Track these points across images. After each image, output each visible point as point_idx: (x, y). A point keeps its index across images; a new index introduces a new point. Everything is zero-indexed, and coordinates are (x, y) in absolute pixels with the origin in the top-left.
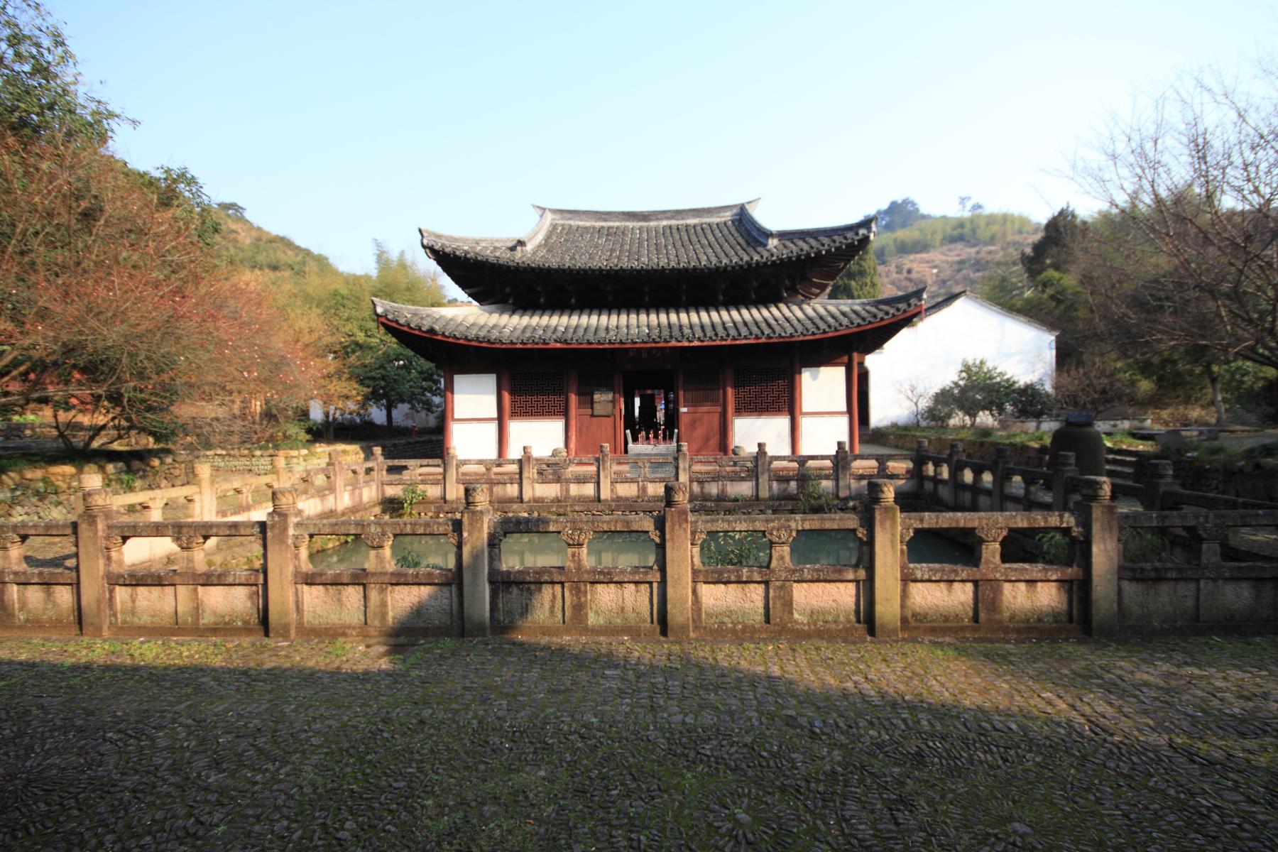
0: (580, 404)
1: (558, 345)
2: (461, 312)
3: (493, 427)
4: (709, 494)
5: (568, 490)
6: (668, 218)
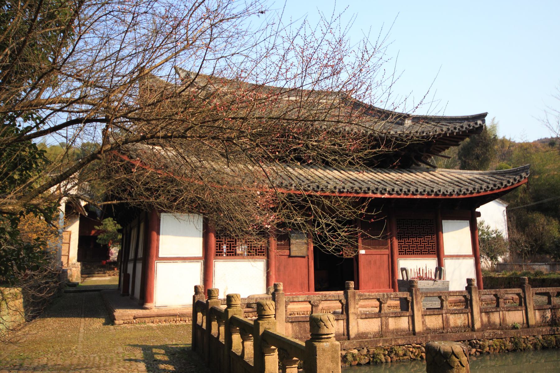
0: (279, 247)
3: (198, 267)
5: (387, 325)
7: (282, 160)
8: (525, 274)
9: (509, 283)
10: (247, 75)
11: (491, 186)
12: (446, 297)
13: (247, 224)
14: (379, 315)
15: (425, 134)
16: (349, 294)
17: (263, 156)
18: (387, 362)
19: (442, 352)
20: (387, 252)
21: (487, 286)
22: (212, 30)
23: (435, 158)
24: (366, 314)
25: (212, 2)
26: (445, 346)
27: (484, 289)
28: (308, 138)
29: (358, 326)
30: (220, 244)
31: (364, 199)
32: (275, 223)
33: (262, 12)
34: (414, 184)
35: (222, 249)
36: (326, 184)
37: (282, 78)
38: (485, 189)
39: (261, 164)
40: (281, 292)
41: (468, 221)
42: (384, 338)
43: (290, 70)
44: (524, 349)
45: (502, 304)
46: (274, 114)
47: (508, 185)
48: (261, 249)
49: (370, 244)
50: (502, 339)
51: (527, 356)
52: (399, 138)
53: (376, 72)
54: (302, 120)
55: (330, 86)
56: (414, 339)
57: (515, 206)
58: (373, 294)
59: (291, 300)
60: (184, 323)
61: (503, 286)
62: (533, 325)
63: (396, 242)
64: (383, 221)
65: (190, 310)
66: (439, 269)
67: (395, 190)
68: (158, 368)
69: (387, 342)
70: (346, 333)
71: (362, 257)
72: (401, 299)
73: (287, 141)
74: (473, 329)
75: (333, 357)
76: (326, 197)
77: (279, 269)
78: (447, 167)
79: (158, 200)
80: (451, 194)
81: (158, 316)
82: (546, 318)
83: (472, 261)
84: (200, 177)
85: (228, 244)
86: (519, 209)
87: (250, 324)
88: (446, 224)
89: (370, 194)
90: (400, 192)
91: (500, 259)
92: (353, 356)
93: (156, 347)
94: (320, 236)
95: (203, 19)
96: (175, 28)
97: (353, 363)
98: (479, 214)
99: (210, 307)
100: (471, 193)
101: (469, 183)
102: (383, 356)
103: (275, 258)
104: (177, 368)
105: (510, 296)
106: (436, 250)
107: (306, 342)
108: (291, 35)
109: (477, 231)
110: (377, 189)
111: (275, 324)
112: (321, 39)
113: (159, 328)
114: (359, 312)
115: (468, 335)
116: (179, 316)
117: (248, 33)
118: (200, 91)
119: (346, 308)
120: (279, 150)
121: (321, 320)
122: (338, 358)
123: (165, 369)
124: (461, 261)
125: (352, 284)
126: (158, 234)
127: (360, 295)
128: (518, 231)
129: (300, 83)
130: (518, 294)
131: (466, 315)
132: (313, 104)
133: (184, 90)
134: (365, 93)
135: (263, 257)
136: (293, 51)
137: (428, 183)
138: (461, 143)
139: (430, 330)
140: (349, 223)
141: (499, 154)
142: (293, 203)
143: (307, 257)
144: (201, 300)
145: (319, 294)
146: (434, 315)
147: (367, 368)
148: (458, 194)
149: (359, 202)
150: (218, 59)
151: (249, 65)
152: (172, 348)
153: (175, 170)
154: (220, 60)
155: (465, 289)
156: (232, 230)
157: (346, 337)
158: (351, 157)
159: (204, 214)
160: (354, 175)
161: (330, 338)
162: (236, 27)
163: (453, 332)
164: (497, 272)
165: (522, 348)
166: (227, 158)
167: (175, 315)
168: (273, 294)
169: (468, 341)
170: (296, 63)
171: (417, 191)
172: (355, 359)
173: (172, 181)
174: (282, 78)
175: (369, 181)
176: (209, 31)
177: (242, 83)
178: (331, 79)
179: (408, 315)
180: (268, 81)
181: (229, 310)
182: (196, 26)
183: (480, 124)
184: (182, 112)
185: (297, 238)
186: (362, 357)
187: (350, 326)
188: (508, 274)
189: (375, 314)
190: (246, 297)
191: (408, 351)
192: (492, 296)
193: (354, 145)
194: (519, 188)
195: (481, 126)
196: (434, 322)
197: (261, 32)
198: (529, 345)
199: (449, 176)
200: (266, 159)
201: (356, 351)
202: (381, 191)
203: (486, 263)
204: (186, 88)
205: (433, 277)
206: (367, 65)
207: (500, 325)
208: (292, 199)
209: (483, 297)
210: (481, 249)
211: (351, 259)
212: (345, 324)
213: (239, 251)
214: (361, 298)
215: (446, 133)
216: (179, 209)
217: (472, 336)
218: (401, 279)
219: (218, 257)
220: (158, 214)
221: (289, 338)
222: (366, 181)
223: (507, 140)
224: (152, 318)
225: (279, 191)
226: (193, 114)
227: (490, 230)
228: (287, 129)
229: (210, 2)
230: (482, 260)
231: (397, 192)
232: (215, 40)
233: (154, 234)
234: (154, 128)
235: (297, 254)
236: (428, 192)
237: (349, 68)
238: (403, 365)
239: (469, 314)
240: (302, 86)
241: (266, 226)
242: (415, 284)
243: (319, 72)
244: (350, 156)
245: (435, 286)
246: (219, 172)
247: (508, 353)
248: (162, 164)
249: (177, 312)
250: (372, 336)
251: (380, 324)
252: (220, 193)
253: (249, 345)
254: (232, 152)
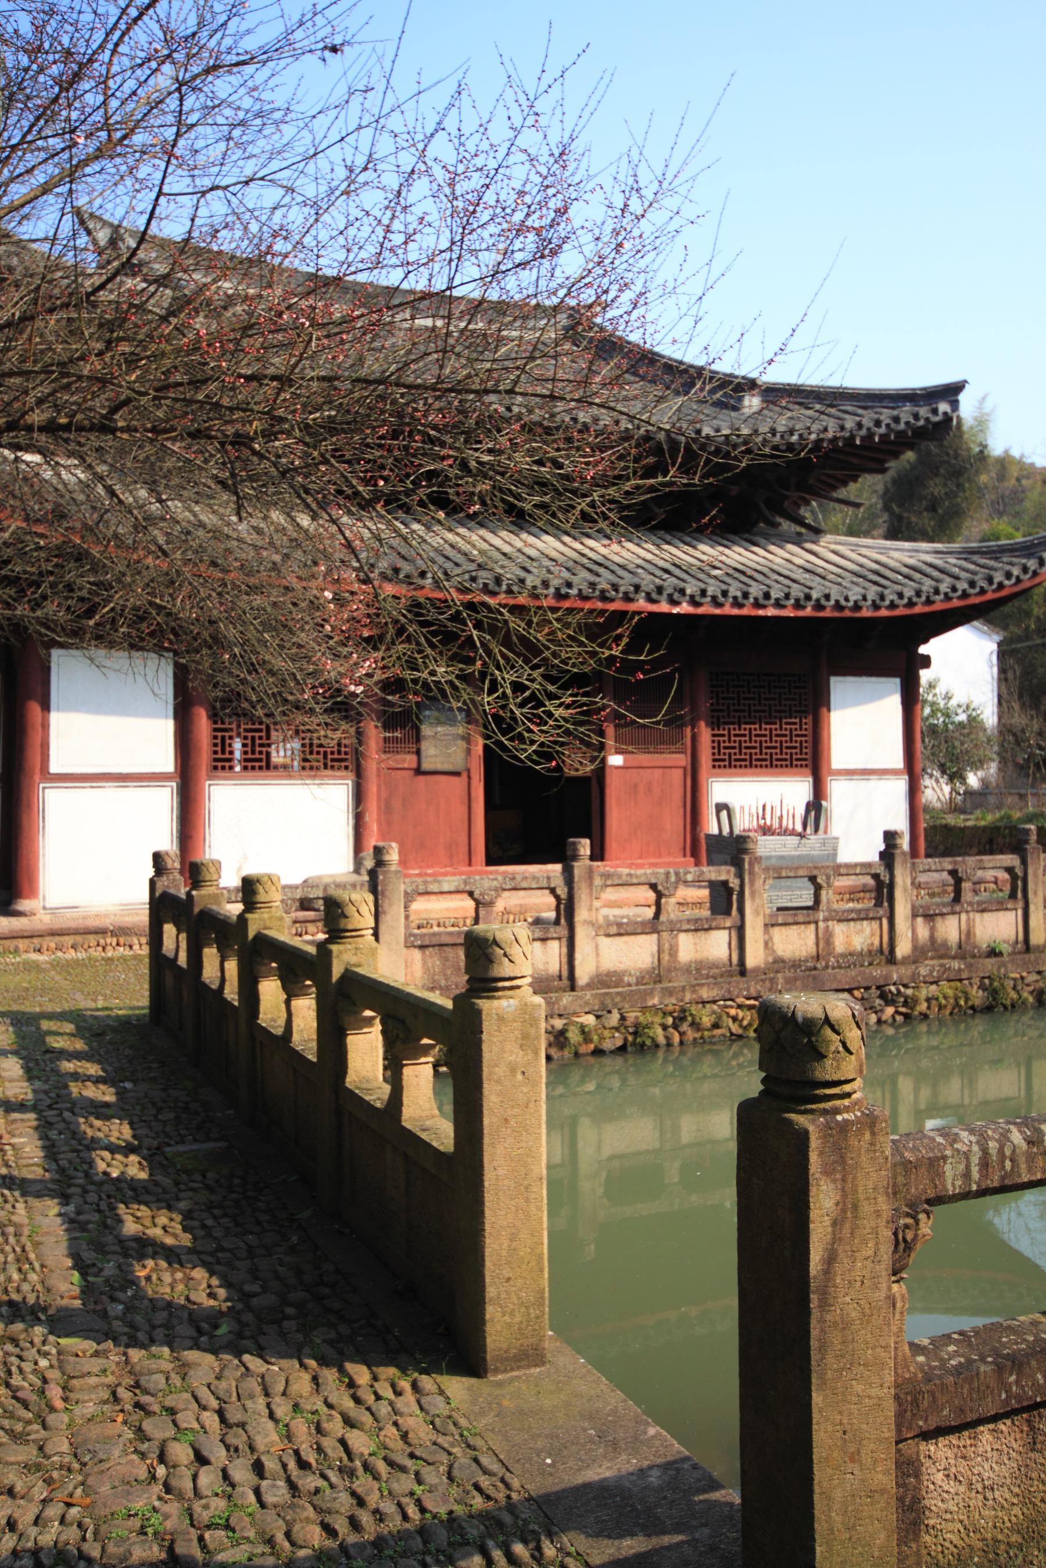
0: (389, 746)
3: (162, 801)
4: (945, 944)
5: (673, 951)
7: (395, 503)
8: (1030, 819)
9: (991, 841)
10: (289, 247)
11: (962, 586)
12: (828, 877)
13: (298, 683)
14: (653, 926)
15: (795, 438)
16: (576, 872)
17: (340, 492)
18: (669, 1045)
19: (800, 1019)
20: (683, 760)
21: (936, 848)
22: (181, 100)
23: (820, 505)
24: (619, 925)
25: (179, 6)
26: (806, 1003)
27: (928, 856)
28: (466, 441)
29: (598, 955)
30: (223, 738)
31: (620, 617)
32: (376, 678)
33: (334, 49)
34: (760, 577)
35: (231, 753)
36: (522, 574)
37: (394, 261)
38: (946, 594)
39: (333, 513)
40: (393, 868)
41: (897, 681)
42: (666, 984)
43: (417, 237)
44: (1013, 1006)
45: (967, 895)
46: (372, 367)
47: (1007, 583)
48: (339, 752)
49: (634, 739)
50: (960, 980)
51: (1018, 1021)
52: (725, 448)
53: (661, 257)
54: (451, 390)
55: (531, 291)
56: (741, 986)
57: (1020, 639)
58: (640, 872)
59: (422, 889)
60: (128, 952)
61: (975, 850)
62: (1038, 947)
64: (668, 679)
65: (142, 917)
66: (816, 807)
67: (709, 593)
68: (56, 1072)
70: (565, 974)
71: (615, 772)
72: (713, 885)
73: (406, 448)
74: (891, 959)
75: (525, 1036)
76: (515, 609)
77: (388, 805)
78: (851, 533)
79: (39, 613)
80: (857, 607)
81: (54, 933)
83: (900, 786)
84: (160, 548)
85: (246, 738)
86: (1030, 648)
87: (307, 953)
88: (840, 687)
89: (641, 604)
90: (721, 599)
91: (973, 780)
92: (583, 1032)
93: (51, 1016)
94: (497, 718)
95: (153, 61)
96: (68, 83)
97: (584, 1049)
98: (926, 662)
99: (196, 910)
100: (911, 604)
101: (906, 577)
102: (659, 1031)
103: (378, 776)
104: (109, 1068)
105: (989, 874)
106: (810, 757)
107: (456, 1000)
108: (419, 129)
109: (919, 706)
110: (660, 590)
111: (373, 953)
112: (508, 144)
113: (55, 965)
114: (601, 920)
115: (877, 972)
116: (113, 934)
117: (293, 116)
118: (152, 289)
119: (567, 909)
120: (386, 473)
121: (495, 942)
122: (538, 1038)
123: (76, 1073)
124: (874, 784)
125: (584, 846)
126: (46, 707)
127: (606, 876)
128: (1023, 706)
129: (446, 279)
130: (1010, 870)
131: (875, 925)
132: (485, 342)
133: (102, 286)
134: (629, 313)
135: (344, 773)
136: (425, 180)
137: (799, 575)
138: (892, 464)
139: (783, 961)
140: (578, 681)
141: (990, 497)
142: (424, 624)
143: (465, 775)
144: (172, 891)
145: (497, 872)
146: (796, 923)
147: (619, 1061)
148: (876, 606)
149: (602, 627)
150: (204, 193)
151: (297, 217)
152: (95, 1018)
153: (85, 526)
154: (208, 196)
155: (877, 858)
156: (254, 698)
157: (565, 982)
158: (588, 500)
159: (176, 653)
160: (596, 547)
161: (518, 987)
162: (255, 94)
163: (840, 967)
164: (963, 811)
165: (1008, 1002)
166: (236, 494)
167: (101, 932)
168: (373, 874)
169: (878, 988)
170: (433, 217)
171: (767, 595)
172: (587, 1040)
173: (81, 557)
174: (394, 261)
175: (638, 566)
176: (173, 103)
177: (280, 269)
178: (535, 270)
179: (728, 924)
180: (352, 269)
181: (248, 916)
182: (131, 85)
183: (945, 413)
184: (100, 354)
185: (439, 723)
186: (607, 1033)
187: (578, 956)
188: (990, 818)
189: (643, 924)
190: (298, 881)
191: (725, 1017)
192: (945, 874)
193: (596, 463)
194: (1036, 591)
195: (948, 419)
196: (795, 942)
197: (333, 113)
198: (1025, 995)
199: (854, 556)
200: (347, 497)
201: (590, 1020)
202: (670, 596)
203: (936, 791)
204: (109, 280)
205: (799, 828)
206: (636, 233)
207: (960, 947)
208: (422, 615)
209: (923, 878)
210: (928, 752)
211: (584, 780)
212: (565, 950)
213: (278, 757)
214: (609, 882)
215: (852, 437)
216: (104, 638)
217: (888, 976)
218: (715, 831)
219: (220, 773)
220: (42, 652)
221: (410, 989)
222: (631, 567)
223: (1013, 458)
224: (36, 940)
225: (389, 589)
226: (131, 362)
227: (953, 703)
228: (414, 409)
229: (176, 5)
230: (927, 781)
231: (714, 598)
232: (192, 134)
233: (35, 708)
234: (16, 399)
235: (440, 767)
236: (797, 600)
237: (586, 238)
238: (709, 1050)
239: (885, 921)
240: (449, 288)
241: (352, 688)
242: (751, 846)
243: (501, 246)
244: (584, 496)
245: (803, 851)
246: (216, 534)
247: (972, 1016)
248: (49, 507)
249: (107, 923)
250: (633, 980)
251: (655, 948)
252: (220, 594)
253: (306, 1008)
254: (251, 479)
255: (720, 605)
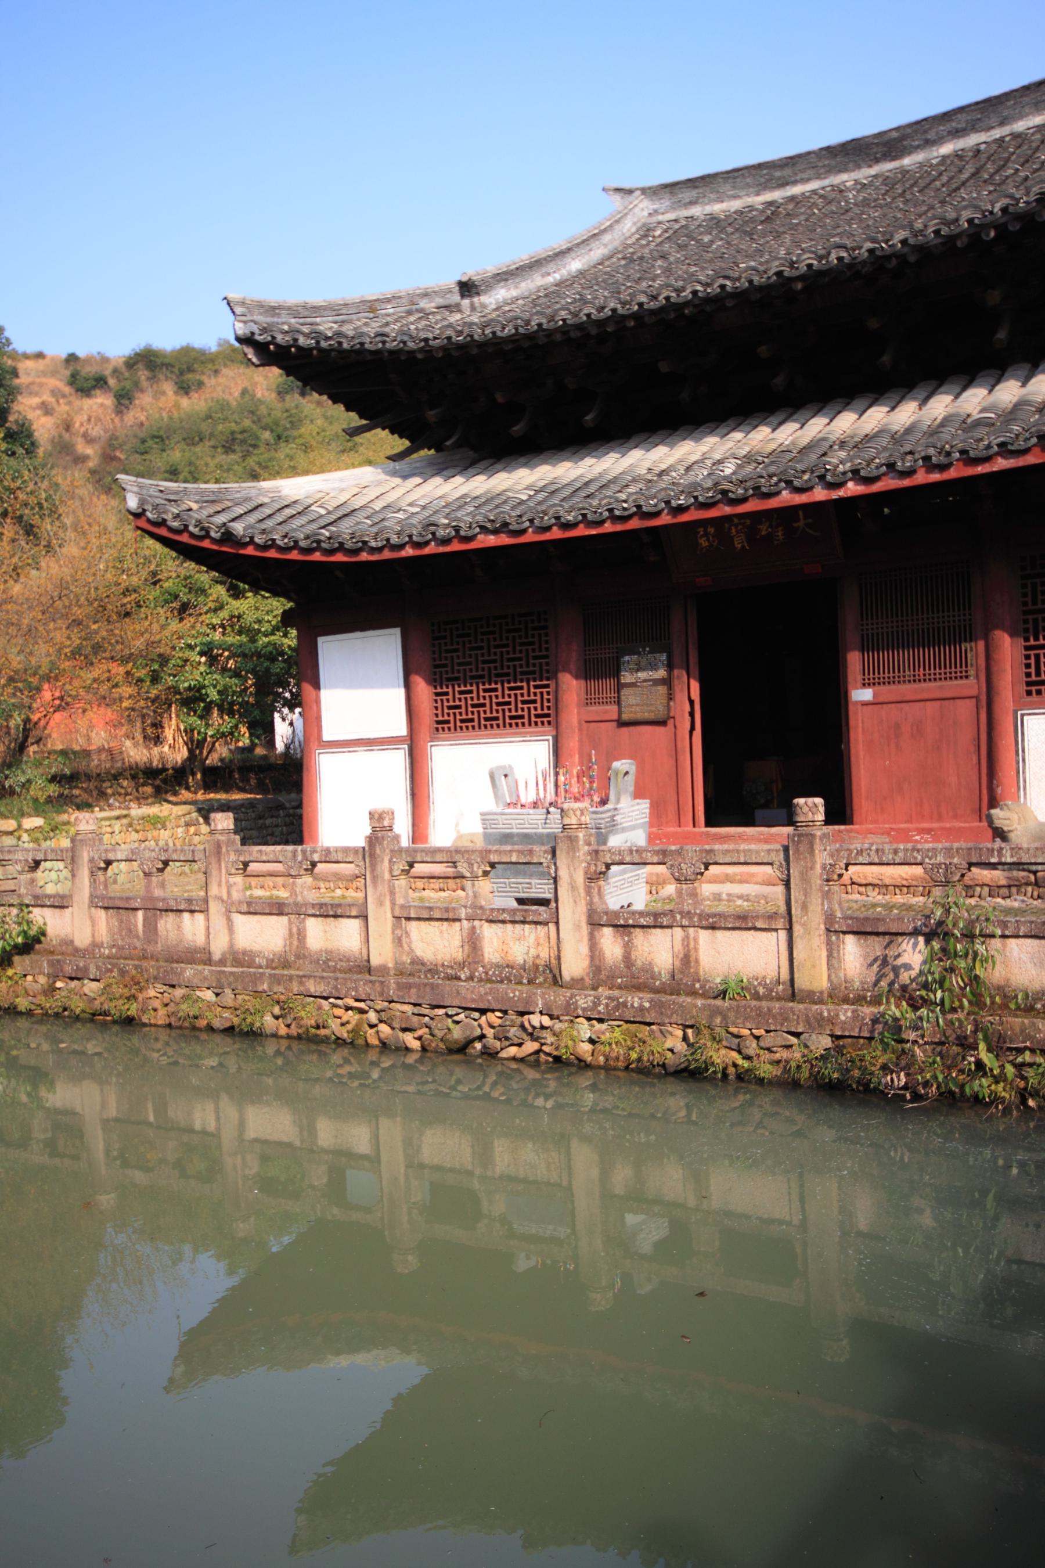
1: (492, 540)
2: (358, 488)
3: (398, 759)
4: (648, 969)
5: (301, 936)
6: (958, 133)
20: (972, 685)
63: (1009, 648)
69: (279, 984)
82: (896, 970)
139: (423, 964)
163: (489, 980)
219: (441, 735)
224: (261, 879)
235: (639, 716)
250: (264, 963)
255: (942, 468)
